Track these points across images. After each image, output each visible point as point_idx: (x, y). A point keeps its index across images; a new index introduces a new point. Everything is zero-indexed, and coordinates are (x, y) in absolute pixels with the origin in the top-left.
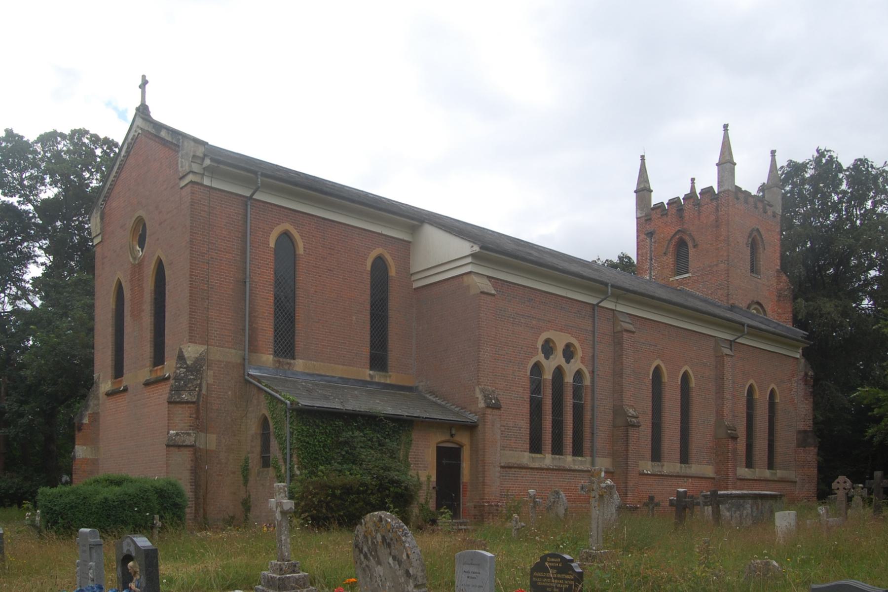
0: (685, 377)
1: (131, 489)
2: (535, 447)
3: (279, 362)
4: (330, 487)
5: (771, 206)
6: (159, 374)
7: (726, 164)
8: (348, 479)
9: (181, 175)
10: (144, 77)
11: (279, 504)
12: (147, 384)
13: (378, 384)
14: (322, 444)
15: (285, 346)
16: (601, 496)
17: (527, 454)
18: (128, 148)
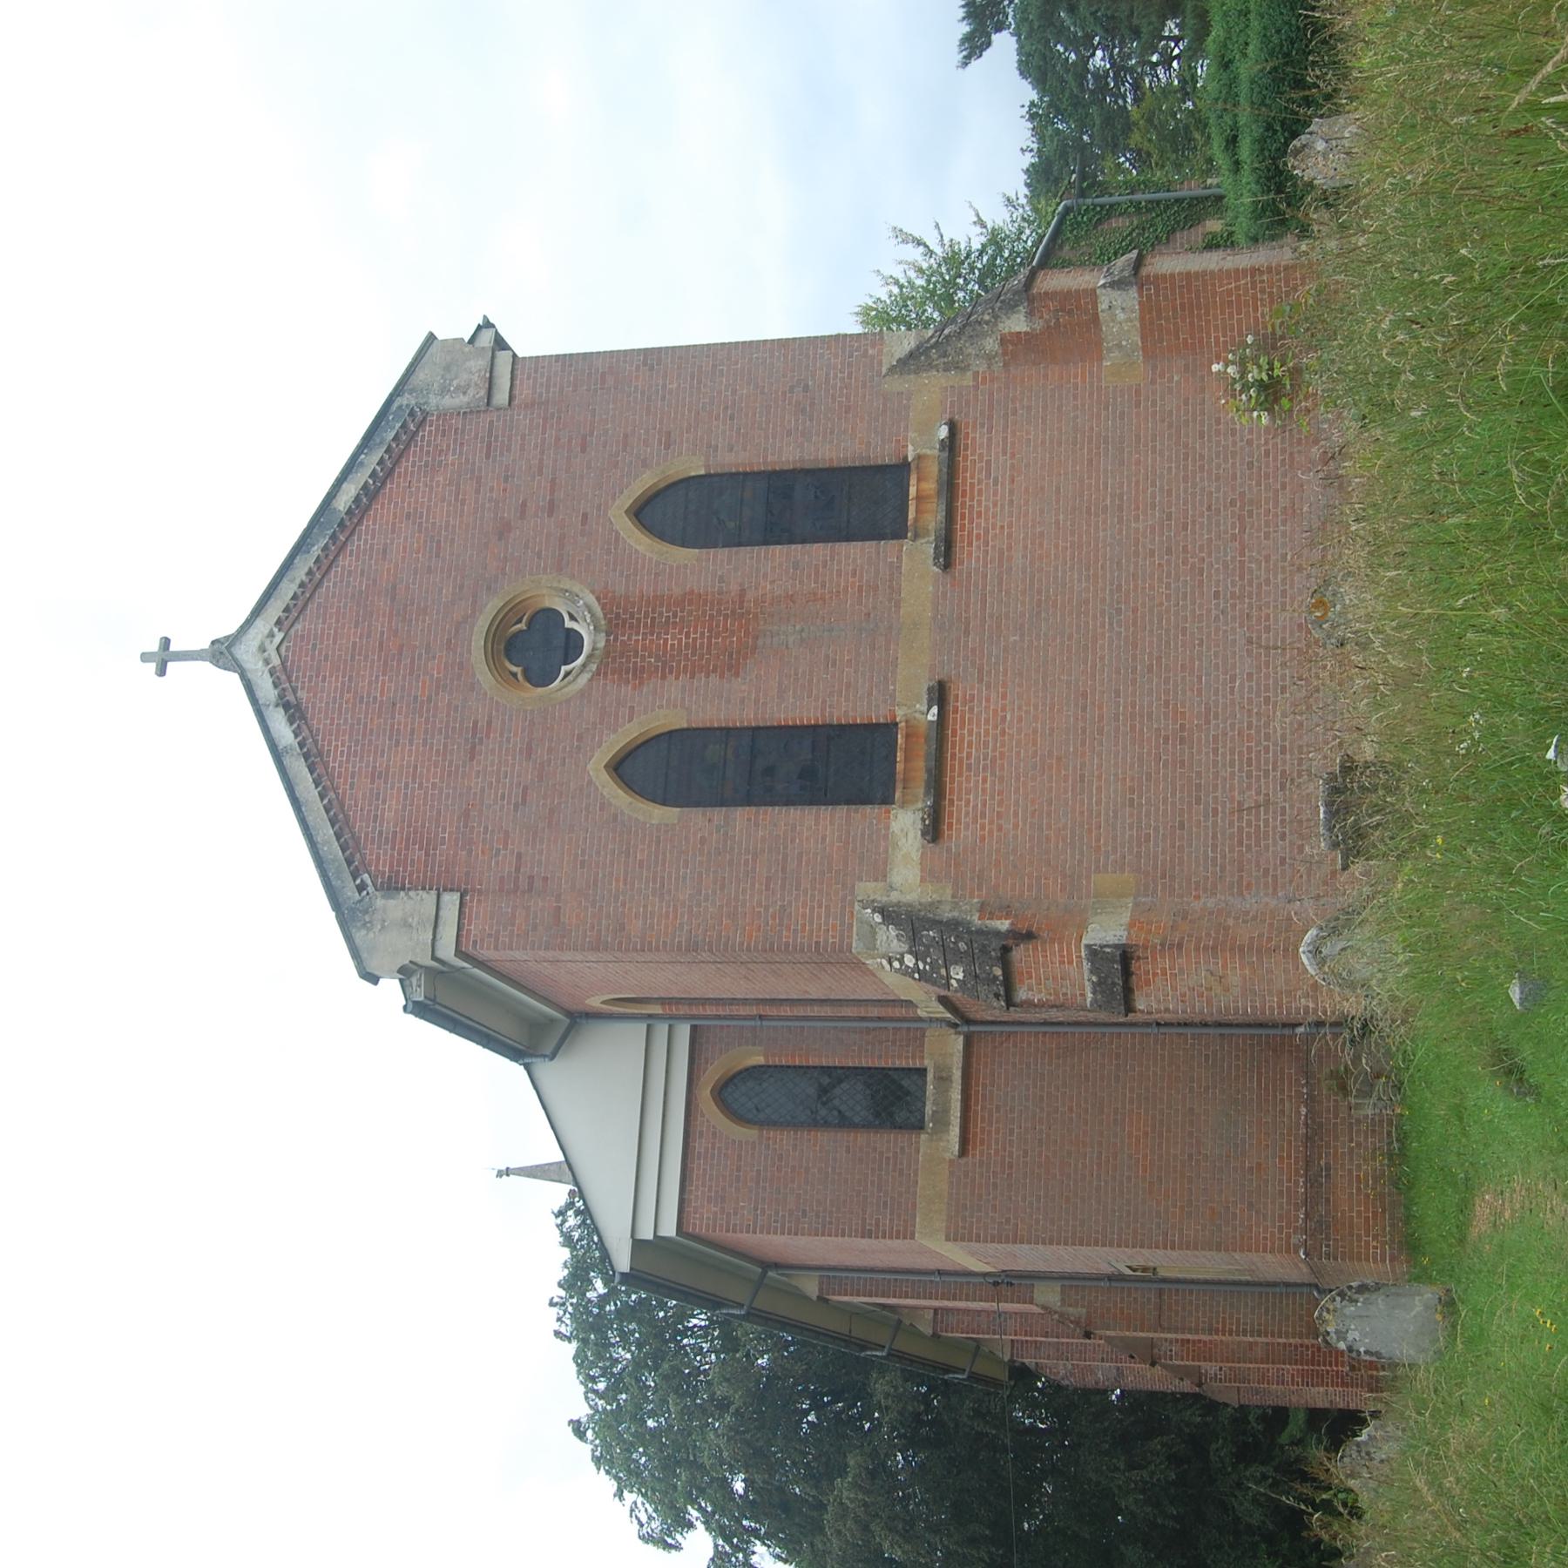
6: (930, 486)
12: (946, 554)
18: (287, 706)
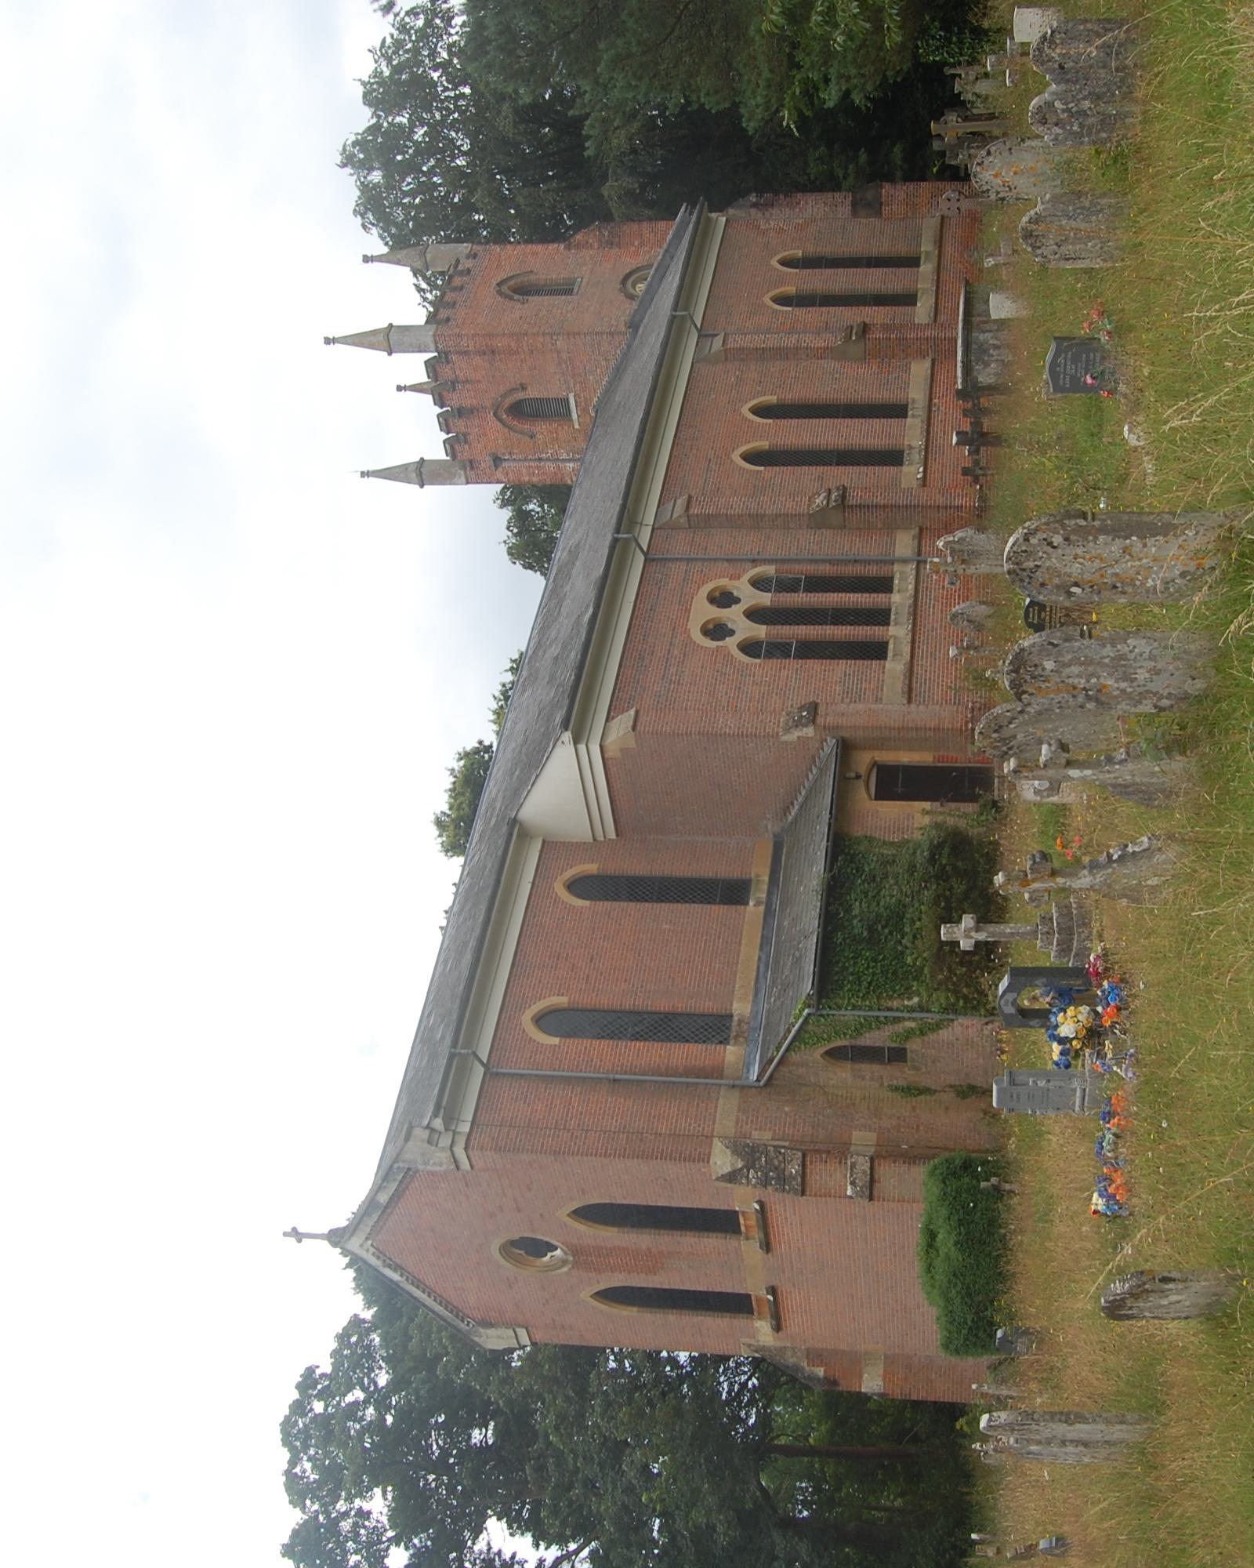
0: (761, 411)
2: (877, 651)
3: (737, 1037)
5: (458, 262)
6: (753, 1222)
7: (389, 339)
9: (453, 1167)
10: (285, 1234)
12: (767, 1247)
13: (770, 894)
14: (872, 964)
15: (715, 1027)
16: (963, 562)
17: (889, 664)
18: (389, 1266)
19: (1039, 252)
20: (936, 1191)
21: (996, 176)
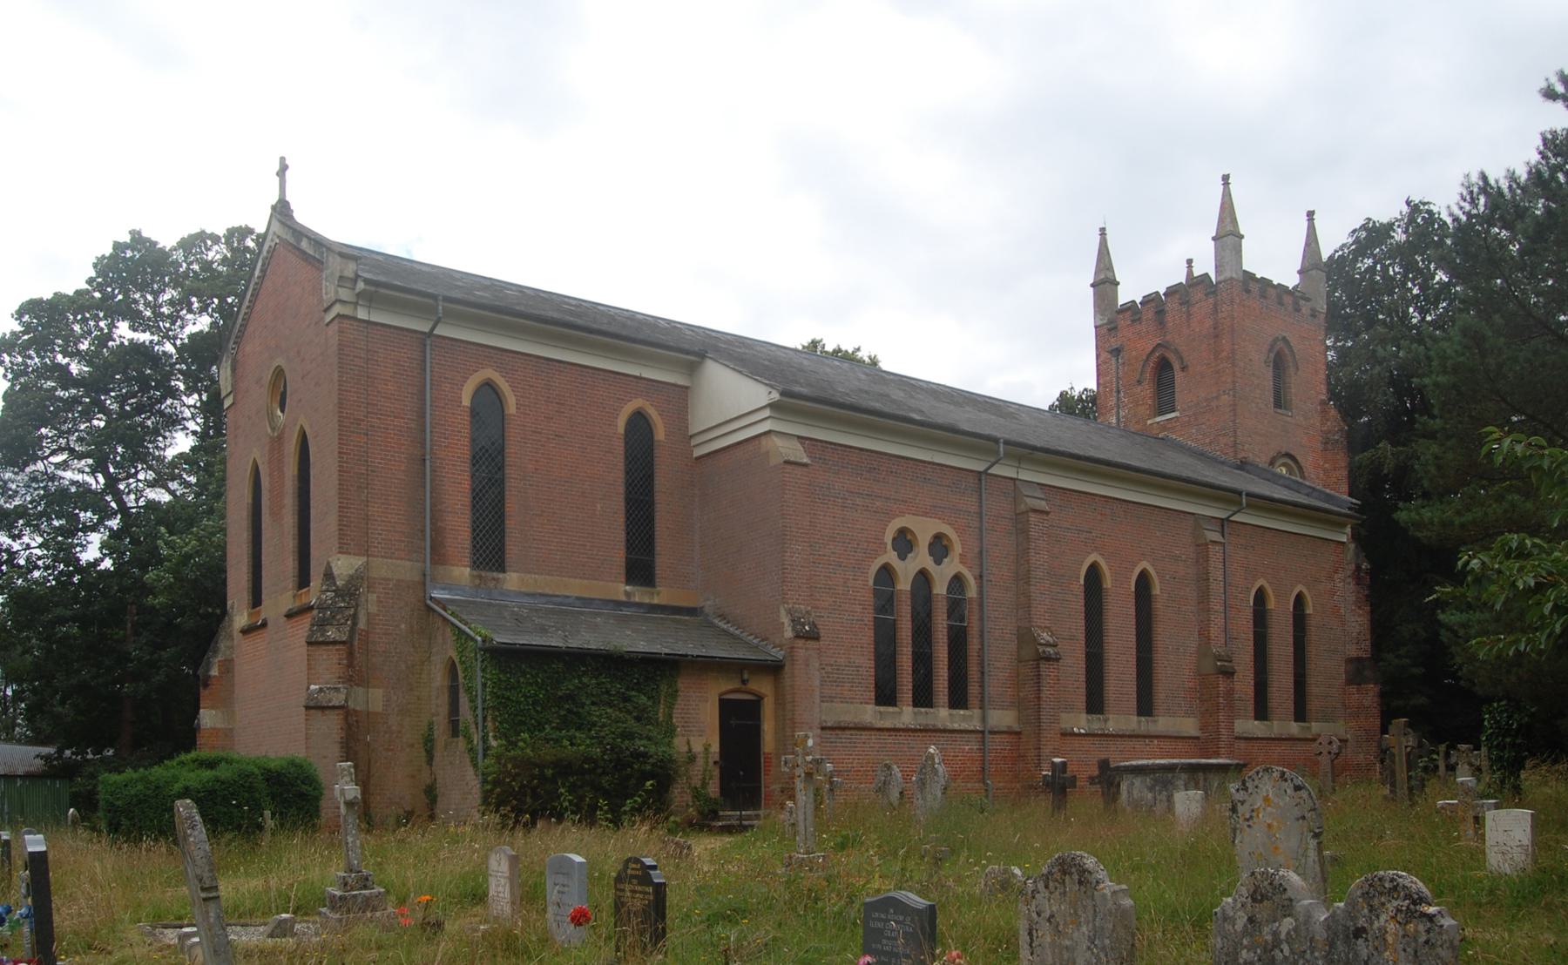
0: (1143, 581)
1: (223, 772)
2: (885, 695)
3: (480, 577)
4: (536, 765)
5: (1308, 300)
6: (304, 600)
7: (1228, 236)
8: (568, 751)
10: (282, 159)
11: (342, 792)
12: (290, 615)
15: (490, 552)
17: (871, 708)
19: (1041, 886)
20: (272, 765)
21: (1266, 799)
